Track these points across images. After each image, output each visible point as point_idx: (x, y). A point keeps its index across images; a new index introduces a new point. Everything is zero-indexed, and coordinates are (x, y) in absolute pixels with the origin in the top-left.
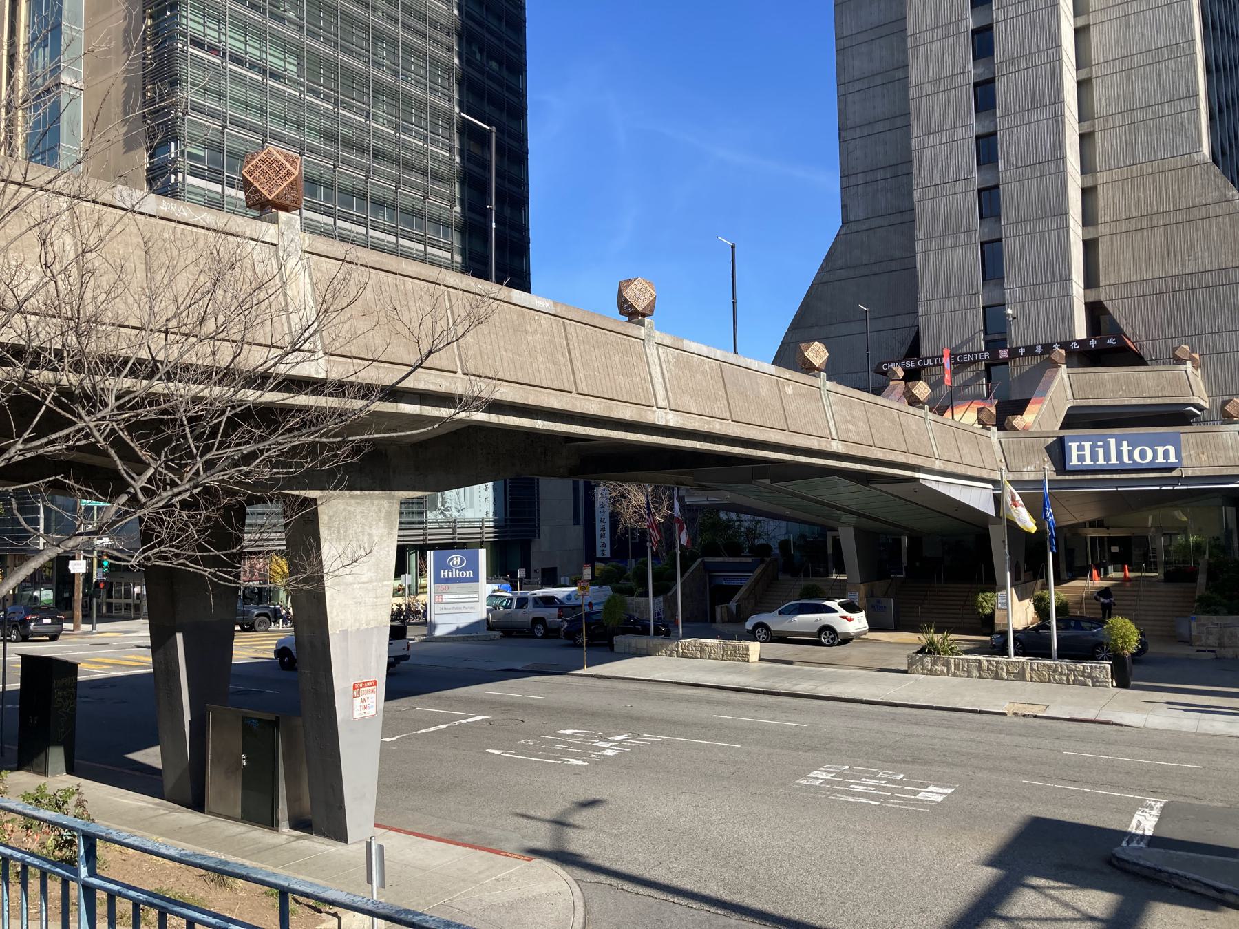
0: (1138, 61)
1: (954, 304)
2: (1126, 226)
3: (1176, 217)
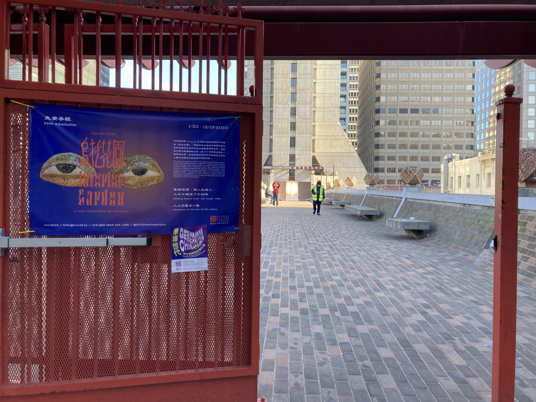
0: (327, 95)
1: (282, 153)
2: (322, 138)
3: (333, 137)
